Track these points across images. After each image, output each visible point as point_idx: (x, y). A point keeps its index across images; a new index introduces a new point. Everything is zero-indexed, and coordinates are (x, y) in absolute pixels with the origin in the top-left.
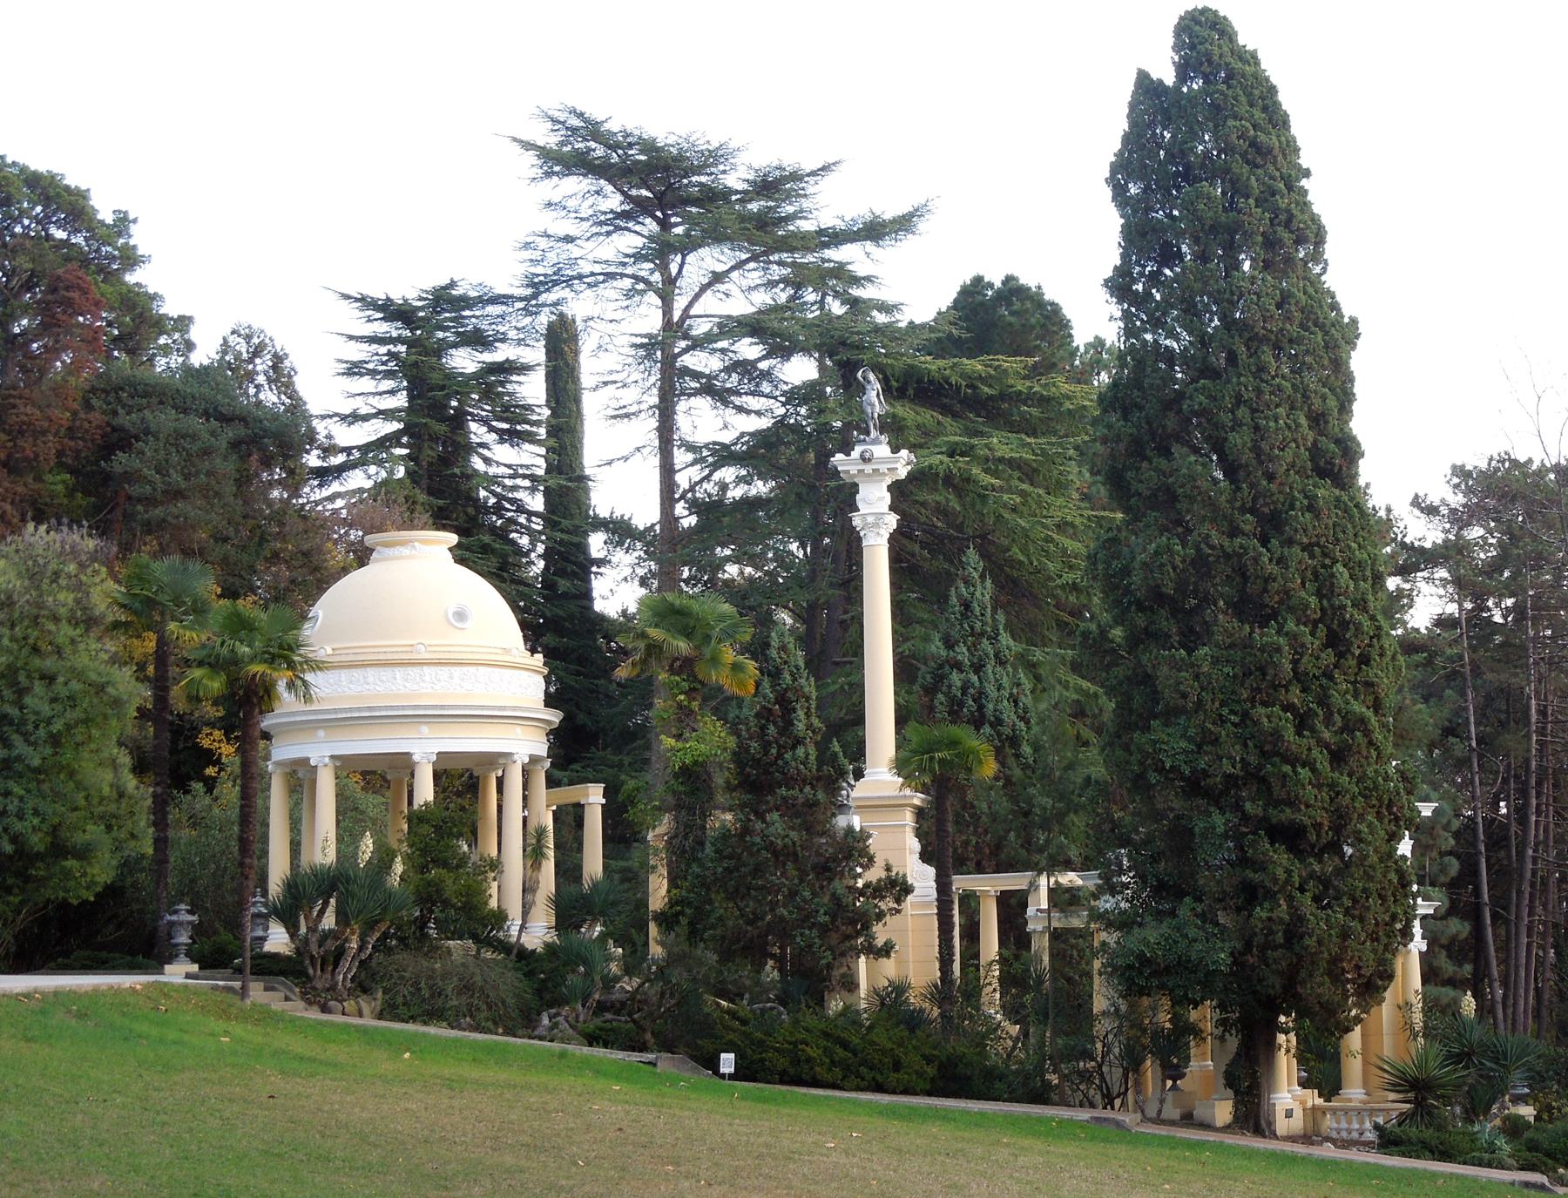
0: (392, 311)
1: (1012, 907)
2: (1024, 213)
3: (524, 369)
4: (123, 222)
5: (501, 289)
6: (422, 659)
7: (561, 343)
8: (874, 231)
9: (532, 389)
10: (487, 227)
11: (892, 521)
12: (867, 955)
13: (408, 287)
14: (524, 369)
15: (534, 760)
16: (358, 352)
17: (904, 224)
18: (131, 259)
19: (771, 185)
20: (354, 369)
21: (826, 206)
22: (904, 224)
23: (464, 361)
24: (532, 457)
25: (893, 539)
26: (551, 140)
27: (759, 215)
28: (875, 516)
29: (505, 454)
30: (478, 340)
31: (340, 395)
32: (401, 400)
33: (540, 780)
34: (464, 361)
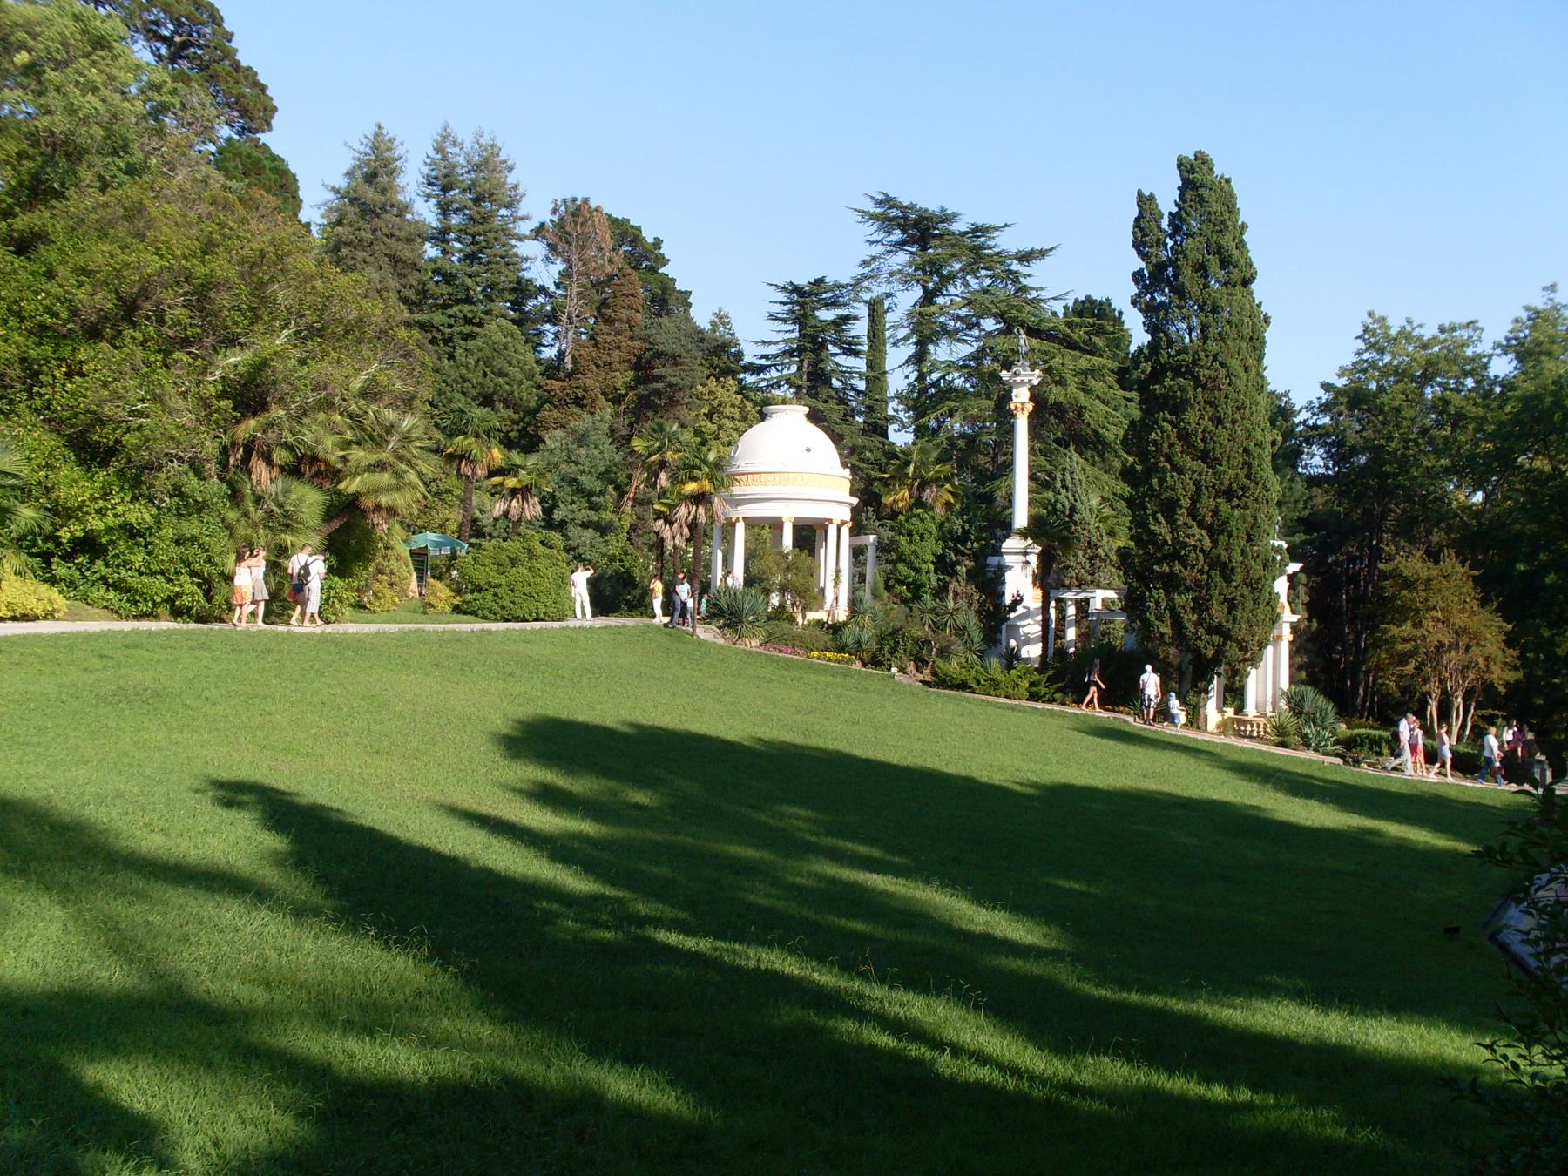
0: (796, 290)
1: (1082, 606)
2: (1089, 262)
3: (856, 318)
4: (658, 243)
5: (844, 282)
6: (790, 467)
7: (876, 310)
8: (1026, 257)
9: (860, 329)
10: (841, 250)
11: (1030, 407)
12: (1046, 401)
13: (802, 280)
14: (856, 318)
15: (843, 523)
16: (777, 308)
17: (1043, 254)
18: (664, 261)
19: (977, 230)
20: (773, 318)
21: (1006, 242)
22: (1043, 254)
23: (826, 315)
24: (860, 364)
25: (1030, 416)
26: (872, 208)
27: (975, 248)
28: (1021, 396)
29: (846, 361)
30: (833, 304)
31: (759, 331)
32: (796, 334)
33: (845, 531)
34: (826, 315)
